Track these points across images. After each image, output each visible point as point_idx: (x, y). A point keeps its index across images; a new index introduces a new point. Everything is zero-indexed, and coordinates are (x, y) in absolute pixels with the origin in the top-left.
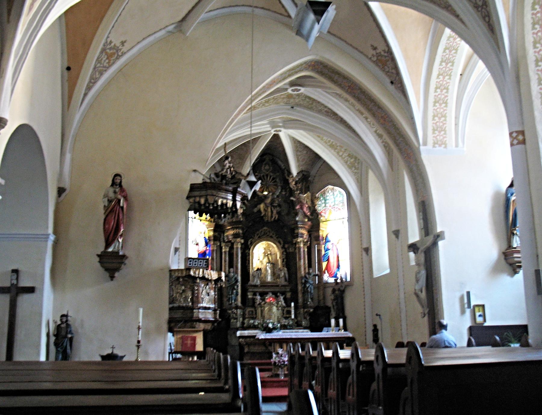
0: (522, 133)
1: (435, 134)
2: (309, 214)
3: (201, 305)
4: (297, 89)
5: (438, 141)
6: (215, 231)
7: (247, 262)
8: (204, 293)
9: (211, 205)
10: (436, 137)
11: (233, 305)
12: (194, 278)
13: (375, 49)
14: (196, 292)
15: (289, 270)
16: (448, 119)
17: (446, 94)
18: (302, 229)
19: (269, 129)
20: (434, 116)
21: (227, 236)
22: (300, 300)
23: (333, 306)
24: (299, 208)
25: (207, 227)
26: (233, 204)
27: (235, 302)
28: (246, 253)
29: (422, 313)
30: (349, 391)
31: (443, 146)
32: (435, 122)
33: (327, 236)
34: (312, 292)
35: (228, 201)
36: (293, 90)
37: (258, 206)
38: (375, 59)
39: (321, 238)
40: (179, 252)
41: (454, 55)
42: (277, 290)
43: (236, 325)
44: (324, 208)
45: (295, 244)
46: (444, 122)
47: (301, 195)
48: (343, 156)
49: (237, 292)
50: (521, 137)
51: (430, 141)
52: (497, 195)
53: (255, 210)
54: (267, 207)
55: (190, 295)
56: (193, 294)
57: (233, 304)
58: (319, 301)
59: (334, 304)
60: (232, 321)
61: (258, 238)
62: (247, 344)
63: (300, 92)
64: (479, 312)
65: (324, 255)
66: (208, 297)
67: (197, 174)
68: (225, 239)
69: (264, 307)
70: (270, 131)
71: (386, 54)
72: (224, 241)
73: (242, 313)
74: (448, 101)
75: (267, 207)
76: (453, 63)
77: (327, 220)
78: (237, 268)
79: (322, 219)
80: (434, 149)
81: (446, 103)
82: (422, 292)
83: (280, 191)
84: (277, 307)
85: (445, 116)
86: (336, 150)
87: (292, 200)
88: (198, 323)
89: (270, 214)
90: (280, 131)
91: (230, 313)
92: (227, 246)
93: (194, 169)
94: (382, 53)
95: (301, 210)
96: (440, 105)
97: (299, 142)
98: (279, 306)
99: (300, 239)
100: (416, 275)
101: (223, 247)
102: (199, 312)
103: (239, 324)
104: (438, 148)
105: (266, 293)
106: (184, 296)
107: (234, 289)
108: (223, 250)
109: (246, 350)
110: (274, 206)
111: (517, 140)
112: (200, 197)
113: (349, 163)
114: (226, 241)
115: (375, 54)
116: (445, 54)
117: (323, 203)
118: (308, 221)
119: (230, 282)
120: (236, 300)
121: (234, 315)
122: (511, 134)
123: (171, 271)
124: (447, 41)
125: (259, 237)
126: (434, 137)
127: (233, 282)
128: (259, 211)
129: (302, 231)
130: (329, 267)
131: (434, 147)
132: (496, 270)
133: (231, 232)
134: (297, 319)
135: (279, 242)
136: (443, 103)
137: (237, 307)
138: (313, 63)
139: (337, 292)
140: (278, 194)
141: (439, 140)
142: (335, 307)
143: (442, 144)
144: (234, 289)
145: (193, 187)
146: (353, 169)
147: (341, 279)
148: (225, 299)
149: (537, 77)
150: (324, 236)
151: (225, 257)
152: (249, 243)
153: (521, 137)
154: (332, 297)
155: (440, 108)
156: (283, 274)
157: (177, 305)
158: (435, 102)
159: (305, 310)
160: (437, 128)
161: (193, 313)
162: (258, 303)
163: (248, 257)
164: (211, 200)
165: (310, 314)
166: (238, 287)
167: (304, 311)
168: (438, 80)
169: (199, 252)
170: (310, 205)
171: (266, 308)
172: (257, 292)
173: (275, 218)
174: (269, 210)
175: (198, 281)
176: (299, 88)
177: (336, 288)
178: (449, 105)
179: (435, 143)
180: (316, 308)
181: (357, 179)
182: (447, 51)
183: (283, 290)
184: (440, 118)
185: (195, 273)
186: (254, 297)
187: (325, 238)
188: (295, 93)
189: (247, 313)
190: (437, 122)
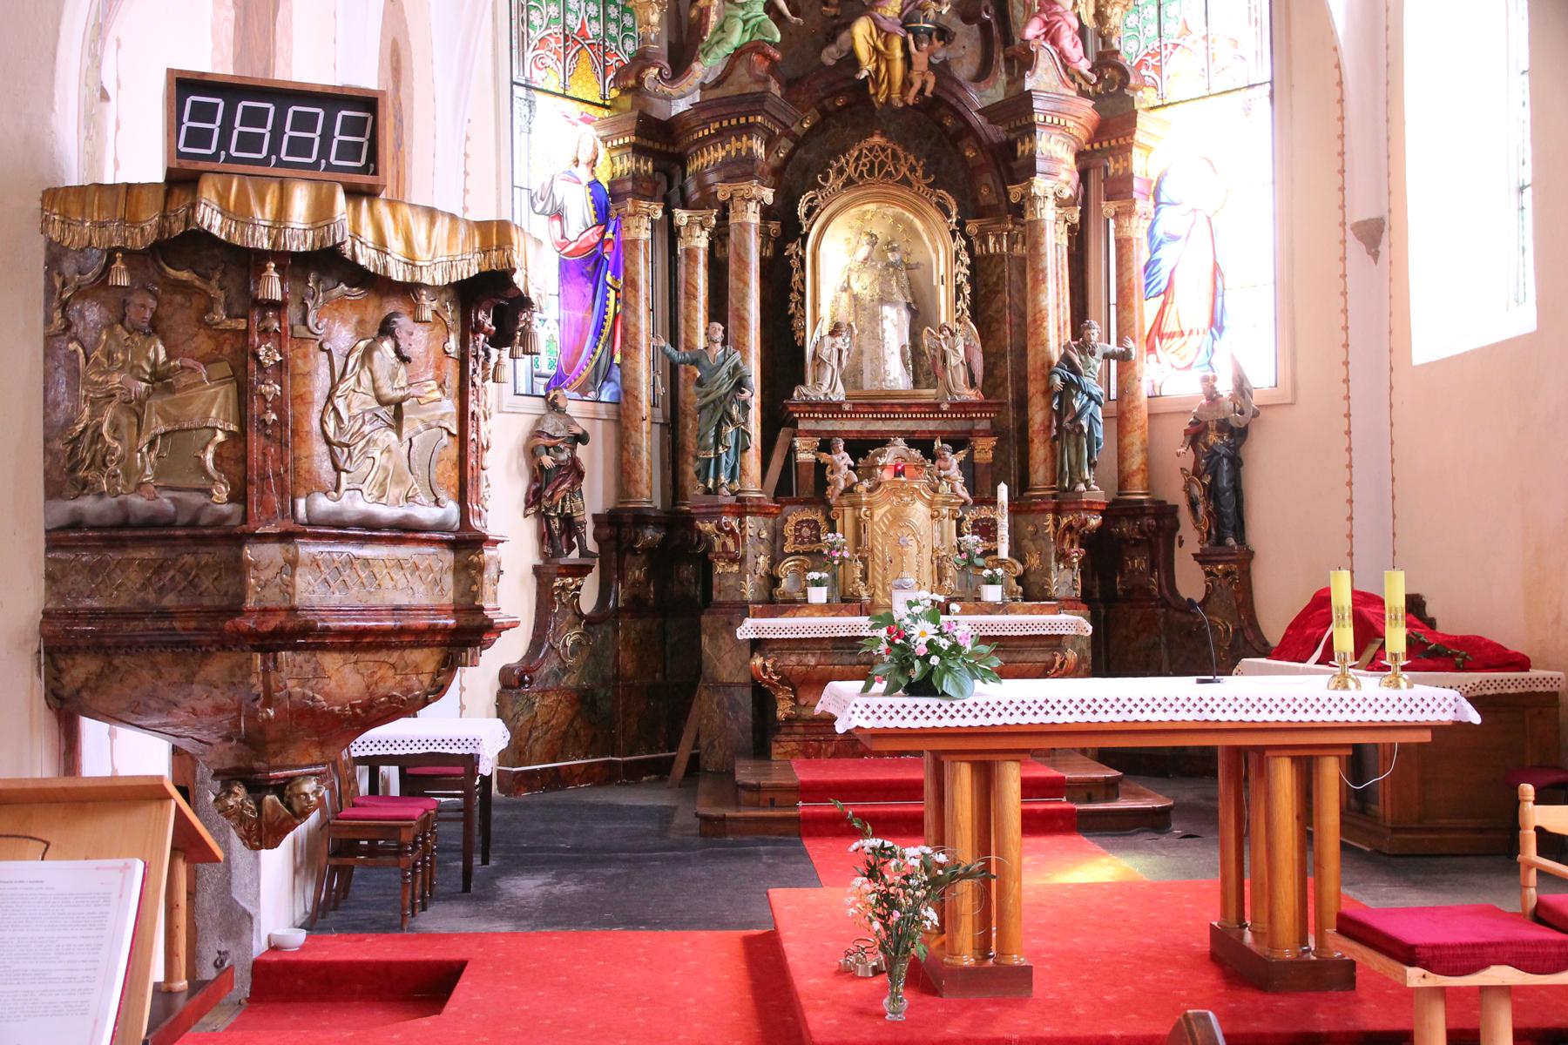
2: (1084, 66)
3: (323, 504)
7: (794, 296)
8: (355, 402)
11: (725, 497)
15: (985, 336)
21: (700, 175)
22: (1040, 474)
23: (1193, 505)
27: (731, 481)
28: (790, 257)
34: (1099, 433)
37: (844, 36)
42: (931, 426)
43: (738, 589)
49: (743, 434)
53: (830, 56)
54: (887, 36)
57: (724, 490)
58: (1123, 481)
59: (1197, 491)
61: (844, 186)
62: (786, 679)
68: (692, 187)
75: (887, 36)
77: (1166, 102)
78: (742, 321)
84: (931, 504)
91: (707, 535)
102: (293, 563)
103: (749, 590)
105: (882, 441)
109: (783, 709)
110: (915, 32)
114: (696, 196)
119: (704, 390)
121: (730, 543)
123: (61, 201)
125: (849, 183)
127: (724, 390)
128: (851, 60)
134: (1023, 562)
137: (742, 508)
139: (1212, 438)
142: (1201, 509)
148: (691, 469)
152: (802, 210)
157: (110, 501)
161: (238, 568)
162: (842, 485)
163: (796, 277)
165: (1091, 542)
166: (745, 407)
167: (1057, 524)
171: (879, 513)
172: (836, 433)
173: (922, 91)
174: (897, 45)
175: (273, 287)
180: (1116, 510)
183: (960, 426)
186: (824, 457)
189: (789, 530)
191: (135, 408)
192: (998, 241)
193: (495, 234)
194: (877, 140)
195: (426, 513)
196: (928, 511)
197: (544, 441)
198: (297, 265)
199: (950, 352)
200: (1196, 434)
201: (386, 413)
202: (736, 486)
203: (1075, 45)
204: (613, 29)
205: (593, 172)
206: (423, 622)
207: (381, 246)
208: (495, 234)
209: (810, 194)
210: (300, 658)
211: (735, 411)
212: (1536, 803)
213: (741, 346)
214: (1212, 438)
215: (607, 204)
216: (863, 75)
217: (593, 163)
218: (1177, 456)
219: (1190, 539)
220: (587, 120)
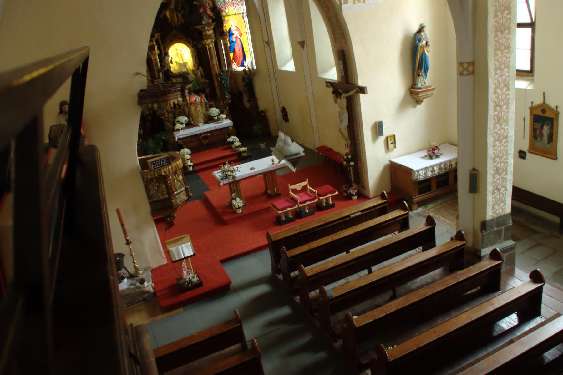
0: (473, 63)
22: (219, 94)
30: (214, 50)
33: (230, 30)
39: (225, 33)
52: (406, 39)
59: (246, 90)
60: (166, 123)
64: (391, 140)
65: (230, 46)
67: (140, 76)
77: (228, 15)
79: (223, 14)
80: (354, 5)
84: (201, 105)
87: (195, 4)
89: (176, 19)
111: (468, 71)
122: (461, 64)
130: (236, 58)
132: (403, 105)
135: (190, 43)
142: (247, 93)
147: (248, 68)
149: (494, 8)
150: (228, 30)
154: (243, 84)
156: (200, 73)
159: (225, 102)
167: (223, 103)
170: (211, 5)
174: (175, 15)
177: (246, 76)
187: (228, 32)
192: (200, 45)
196: (201, 106)
199: (197, 74)
200: (244, 79)
212: (290, 186)
214: (247, 80)
219: (246, 99)
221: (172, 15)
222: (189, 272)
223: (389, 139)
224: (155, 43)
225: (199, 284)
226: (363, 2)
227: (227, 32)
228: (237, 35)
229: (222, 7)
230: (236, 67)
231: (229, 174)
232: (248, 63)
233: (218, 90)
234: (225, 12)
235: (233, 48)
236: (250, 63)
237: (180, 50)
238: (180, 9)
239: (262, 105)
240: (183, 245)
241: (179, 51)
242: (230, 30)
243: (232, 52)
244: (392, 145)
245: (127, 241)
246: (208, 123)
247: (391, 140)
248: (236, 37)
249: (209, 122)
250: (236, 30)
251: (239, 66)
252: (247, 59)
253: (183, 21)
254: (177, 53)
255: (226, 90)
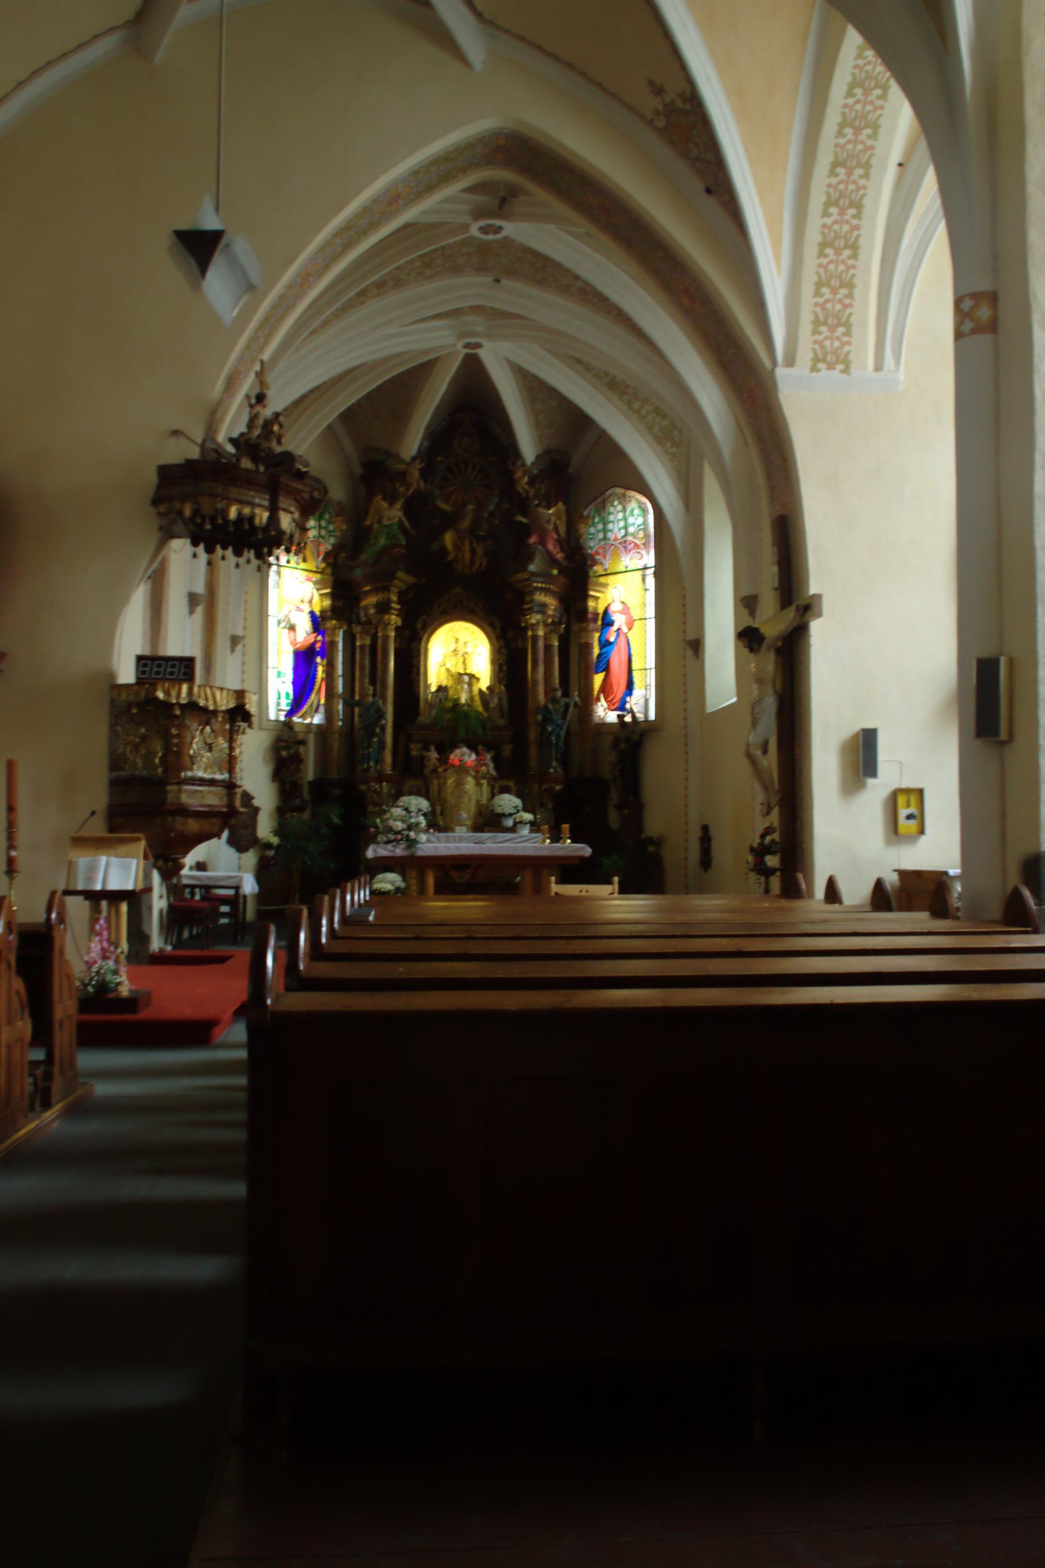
0: (993, 298)
1: (820, 333)
3: (189, 774)
4: (493, 225)
5: (825, 354)
6: (333, 596)
7: (414, 670)
9: (207, 521)
10: (821, 343)
12: (167, 706)
13: (659, 91)
14: (176, 741)
16: (857, 292)
17: (854, 222)
18: (543, 594)
19: (450, 340)
20: (819, 285)
22: (533, 763)
24: (535, 543)
25: (318, 587)
26: (270, 519)
29: (762, 804)
31: (840, 367)
32: (821, 300)
33: (606, 611)
35: (257, 511)
36: (485, 230)
38: (661, 123)
39: (590, 616)
40: (244, 646)
41: (879, 103)
44: (602, 543)
45: (525, 629)
46: (847, 301)
47: (541, 510)
48: (643, 412)
50: (984, 313)
51: (805, 354)
55: (159, 748)
56: (167, 748)
57: (372, 770)
63: (482, 223)
64: (908, 805)
66: (209, 754)
68: (362, 614)
69: (445, 779)
70: (454, 345)
71: (688, 107)
72: (359, 623)
73: (393, 792)
74: (861, 242)
76: (875, 127)
77: (608, 572)
80: (815, 374)
81: (854, 247)
82: (765, 751)
83: (496, 500)
84: (475, 778)
85: (850, 285)
86: (625, 397)
87: (521, 523)
88: (178, 818)
89: (467, 556)
90: (478, 346)
92: (367, 633)
93: (176, 426)
94: (679, 104)
95: (540, 547)
96: (838, 252)
97: (535, 378)
98: (480, 775)
99: (535, 618)
100: (753, 708)
101: (358, 636)
102: (180, 791)
104: (824, 373)
106: (143, 752)
107: (374, 734)
108: (358, 643)
111: (972, 320)
112: (183, 499)
113: (656, 429)
114: (364, 619)
115: (660, 107)
116: (850, 101)
117: (599, 531)
118: (560, 573)
120: (379, 760)
121: (375, 797)
122: (958, 302)
124: (856, 59)
126: (815, 342)
128: (443, 551)
129: (540, 598)
131: (814, 369)
133: (372, 599)
135: (492, 625)
136: (846, 247)
137: (380, 778)
138: (502, 142)
139: (623, 746)
140: (492, 508)
141: (829, 349)
143: (837, 362)
144: (374, 734)
145: (168, 475)
146: (668, 444)
150: (601, 610)
151: (362, 658)
152: (419, 626)
153: (984, 313)
155: (837, 262)
157: (128, 773)
158: (823, 245)
159: (544, 787)
160: (826, 318)
161: (165, 793)
162: (431, 767)
164: (207, 507)
166: (383, 728)
168: (834, 181)
169: (298, 646)
170: (562, 530)
173: (481, 565)
174: (467, 547)
176: (498, 222)
178: (862, 253)
179: (816, 360)
181: (678, 472)
182: (858, 91)
184: (834, 291)
185: (167, 693)
188: (491, 237)
190: (827, 301)
191: (136, 747)
193: (240, 694)
194: (458, 590)
195: (218, 777)
197: (282, 744)
198: (182, 707)
200: (616, 742)
201: (207, 747)
202: (379, 767)
203: (555, 547)
204: (323, 532)
205: (311, 606)
206: (217, 809)
207: (207, 699)
208: (240, 694)
209: (424, 617)
210: (182, 819)
211: (378, 730)
212: (556, 883)
213: (384, 698)
214: (623, 746)
215: (317, 623)
216: (450, 559)
217: (310, 602)
218: (609, 758)
220: (309, 579)
221: (459, 544)
222: (108, 954)
223: (901, 800)
224: (394, 598)
225: (131, 1004)
226: (843, 372)
227: (598, 614)
228: (620, 626)
229: (597, 553)
230: (605, 713)
231: (397, 826)
232: (635, 702)
233: (533, 752)
234: (602, 564)
235: (606, 659)
236: (642, 701)
237: (465, 643)
238: (483, 534)
239: (654, 824)
240: (113, 859)
241: (461, 642)
242: (606, 611)
243: (602, 672)
244: (913, 824)
245: (11, 862)
246: (482, 831)
247: (908, 805)
248: (619, 629)
249: (486, 828)
250: (620, 612)
251: (612, 710)
252: (635, 692)
253: (484, 565)
254: (455, 650)
255: (554, 754)
